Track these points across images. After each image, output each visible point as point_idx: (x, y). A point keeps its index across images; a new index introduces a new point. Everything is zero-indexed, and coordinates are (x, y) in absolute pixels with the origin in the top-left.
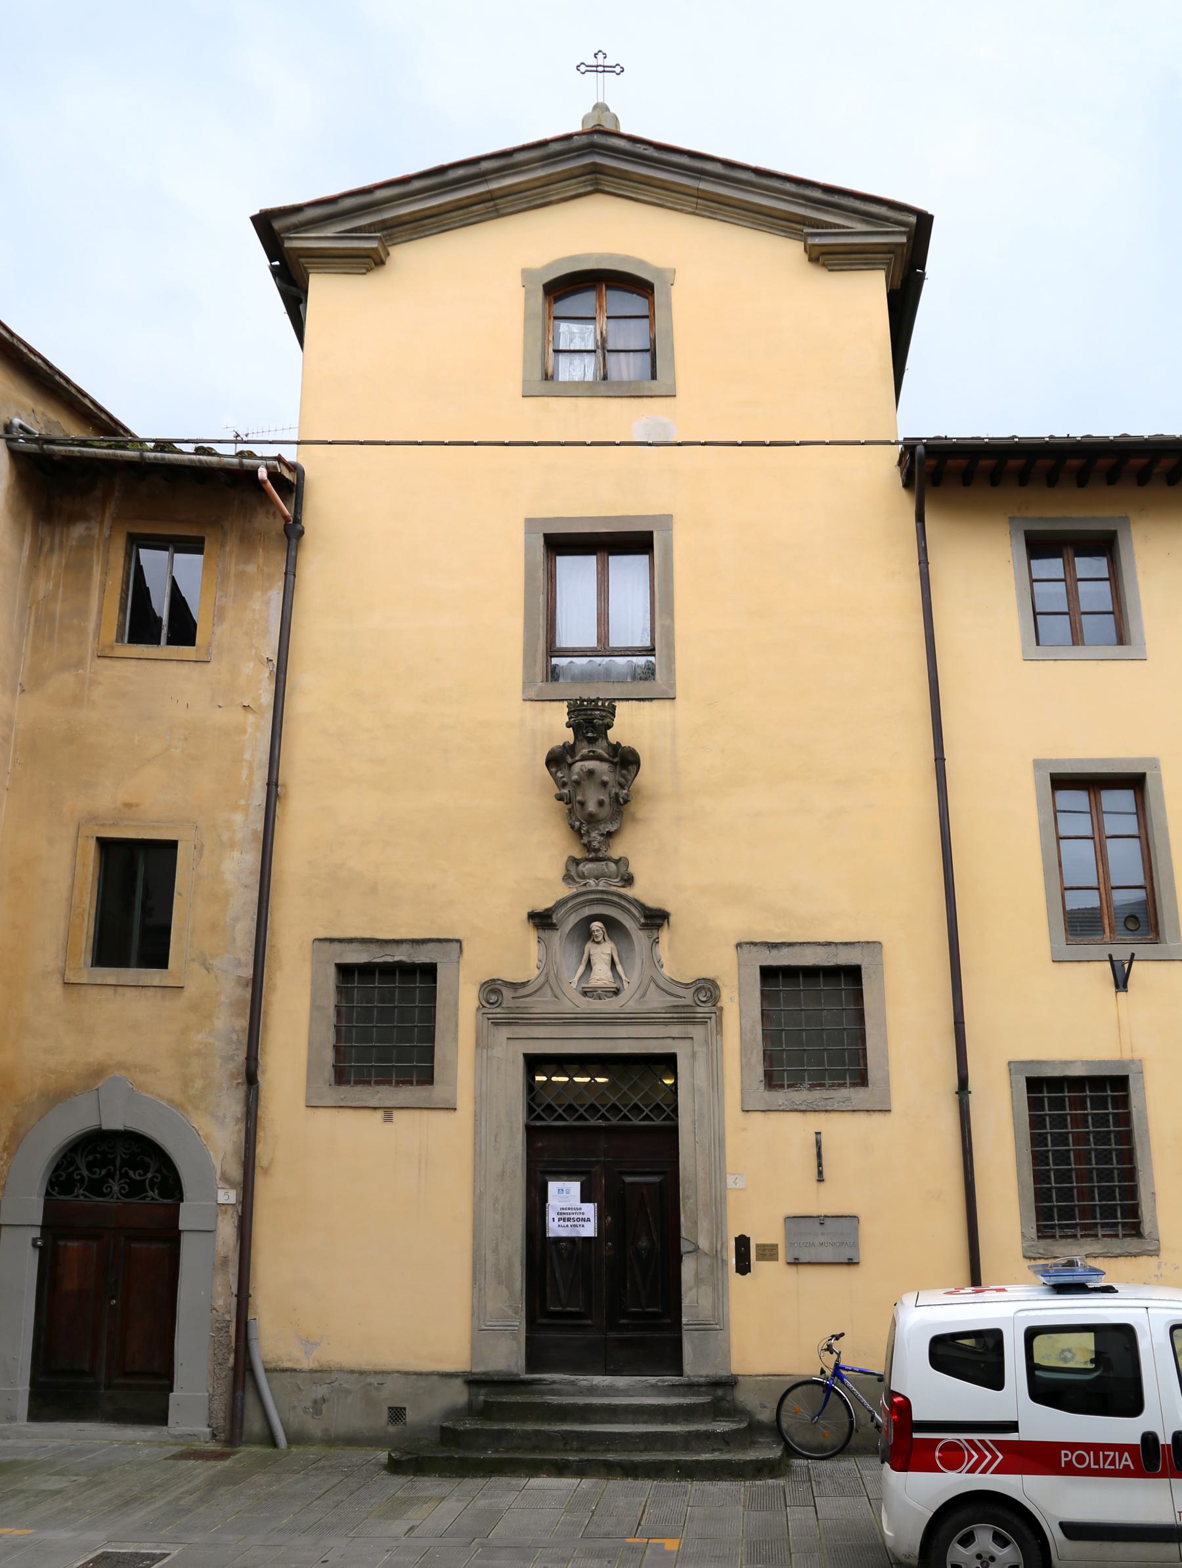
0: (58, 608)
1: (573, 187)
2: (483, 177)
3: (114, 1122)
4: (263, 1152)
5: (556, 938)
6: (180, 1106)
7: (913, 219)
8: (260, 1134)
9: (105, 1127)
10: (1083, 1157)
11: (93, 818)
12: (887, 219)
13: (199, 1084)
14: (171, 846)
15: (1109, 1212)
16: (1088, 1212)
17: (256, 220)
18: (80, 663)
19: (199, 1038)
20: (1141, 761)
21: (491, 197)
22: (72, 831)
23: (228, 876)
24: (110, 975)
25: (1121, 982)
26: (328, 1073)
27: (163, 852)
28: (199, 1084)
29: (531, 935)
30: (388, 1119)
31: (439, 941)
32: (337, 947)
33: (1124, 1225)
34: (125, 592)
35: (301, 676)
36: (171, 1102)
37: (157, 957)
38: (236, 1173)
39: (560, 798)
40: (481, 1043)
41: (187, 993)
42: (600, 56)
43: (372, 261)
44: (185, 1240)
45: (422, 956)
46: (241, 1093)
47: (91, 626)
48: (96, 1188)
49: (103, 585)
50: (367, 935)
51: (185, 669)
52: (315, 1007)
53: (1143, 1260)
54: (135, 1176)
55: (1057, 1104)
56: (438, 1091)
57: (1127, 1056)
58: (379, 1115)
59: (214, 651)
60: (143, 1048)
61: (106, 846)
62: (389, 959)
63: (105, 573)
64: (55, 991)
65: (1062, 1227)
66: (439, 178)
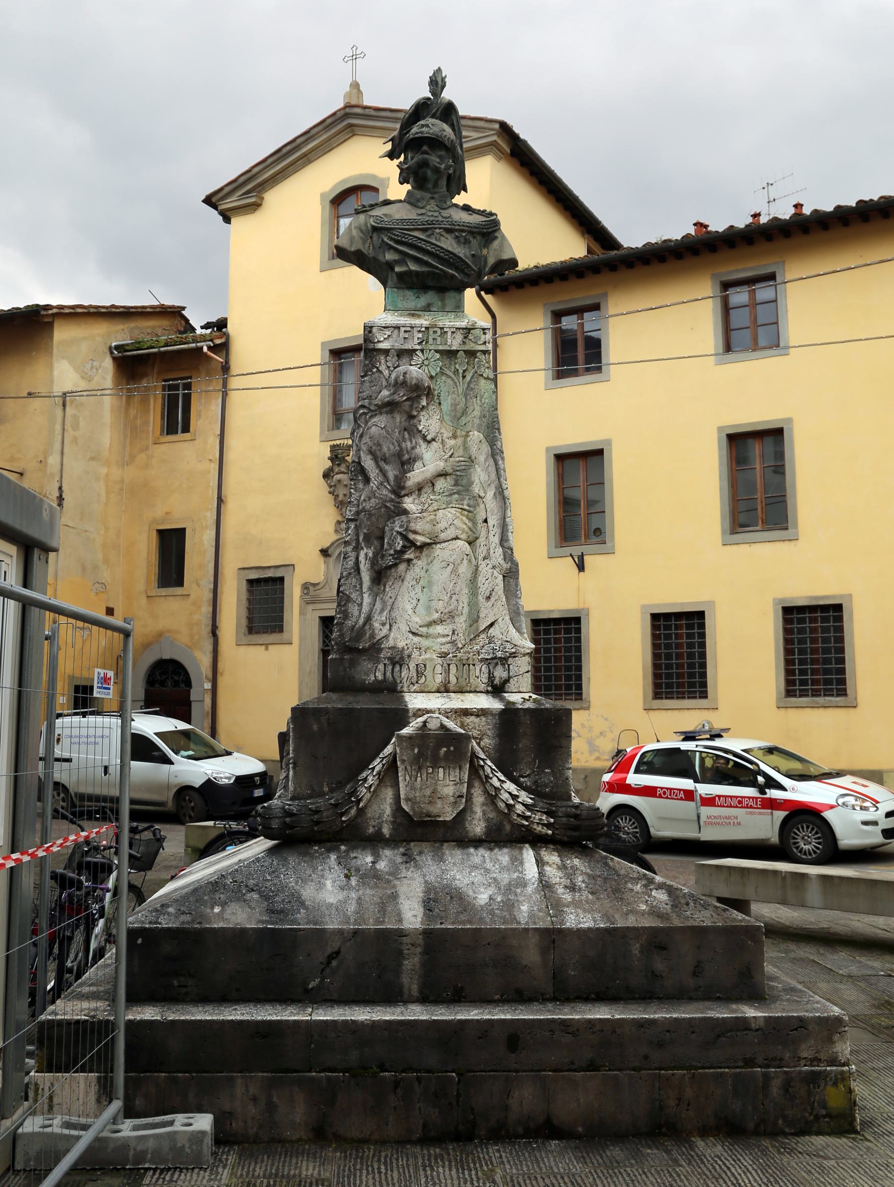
0: (138, 422)
1: (342, 137)
2: (298, 148)
3: (166, 657)
4: (221, 666)
5: (331, 560)
6: (189, 647)
7: (497, 126)
8: (219, 658)
9: (164, 658)
10: (557, 659)
11: (154, 521)
12: (485, 128)
13: (196, 637)
14: (183, 531)
15: (569, 687)
16: (680, 685)
17: (204, 201)
18: (147, 448)
19: (196, 617)
20: (601, 441)
21: (305, 155)
22: (147, 528)
23: (205, 542)
24: (164, 591)
25: (581, 567)
26: (244, 629)
27: (180, 533)
28: (196, 637)
29: (321, 559)
30: (267, 649)
31: (285, 566)
32: (246, 571)
33: (576, 694)
34: (163, 409)
35: (232, 441)
36: (187, 646)
37: (180, 582)
38: (210, 675)
39: (330, 493)
40: (302, 613)
41: (192, 597)
42: (354, 49)
43: (255, 207)
44: (193, 704)
45: (278, 574)
46: (212, 640)
47: (151, 429)
48: (162, 684)
49: (154, 407)
50: (258, 565)
51: (186, 445)
52: (239, 600)
53: (581, 712)
54: (176, 678)
55: (547, 632)
56: (285, 635)
57: (581, 606)
58: (263, 647)
59: (197, 434)
60: (171, 621)
61: (161, 533)
62: (266, 576)
63: (155, 402)
64: (143, 601)
65: (677, 692)
66: (279, 154)
